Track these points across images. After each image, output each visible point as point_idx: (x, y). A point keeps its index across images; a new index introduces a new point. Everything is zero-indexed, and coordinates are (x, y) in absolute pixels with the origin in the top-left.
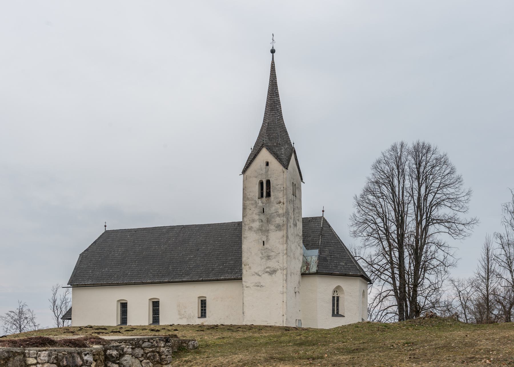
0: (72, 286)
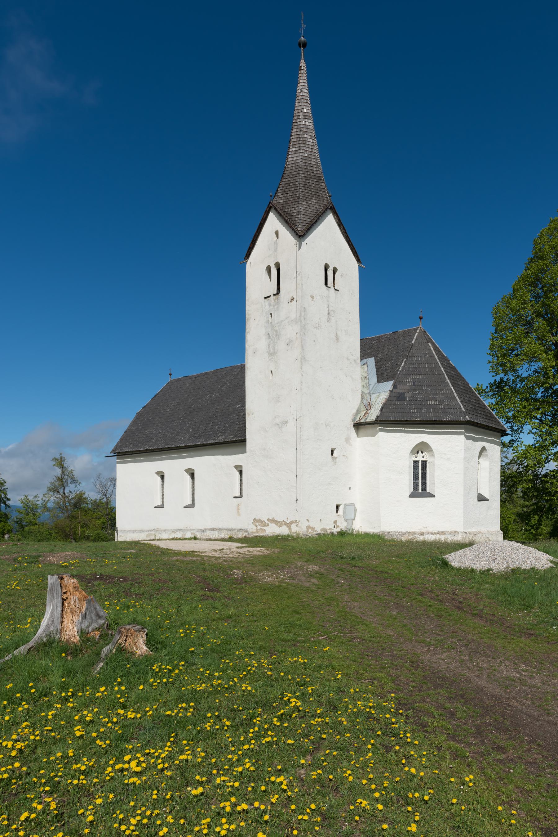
0: (116, 454)
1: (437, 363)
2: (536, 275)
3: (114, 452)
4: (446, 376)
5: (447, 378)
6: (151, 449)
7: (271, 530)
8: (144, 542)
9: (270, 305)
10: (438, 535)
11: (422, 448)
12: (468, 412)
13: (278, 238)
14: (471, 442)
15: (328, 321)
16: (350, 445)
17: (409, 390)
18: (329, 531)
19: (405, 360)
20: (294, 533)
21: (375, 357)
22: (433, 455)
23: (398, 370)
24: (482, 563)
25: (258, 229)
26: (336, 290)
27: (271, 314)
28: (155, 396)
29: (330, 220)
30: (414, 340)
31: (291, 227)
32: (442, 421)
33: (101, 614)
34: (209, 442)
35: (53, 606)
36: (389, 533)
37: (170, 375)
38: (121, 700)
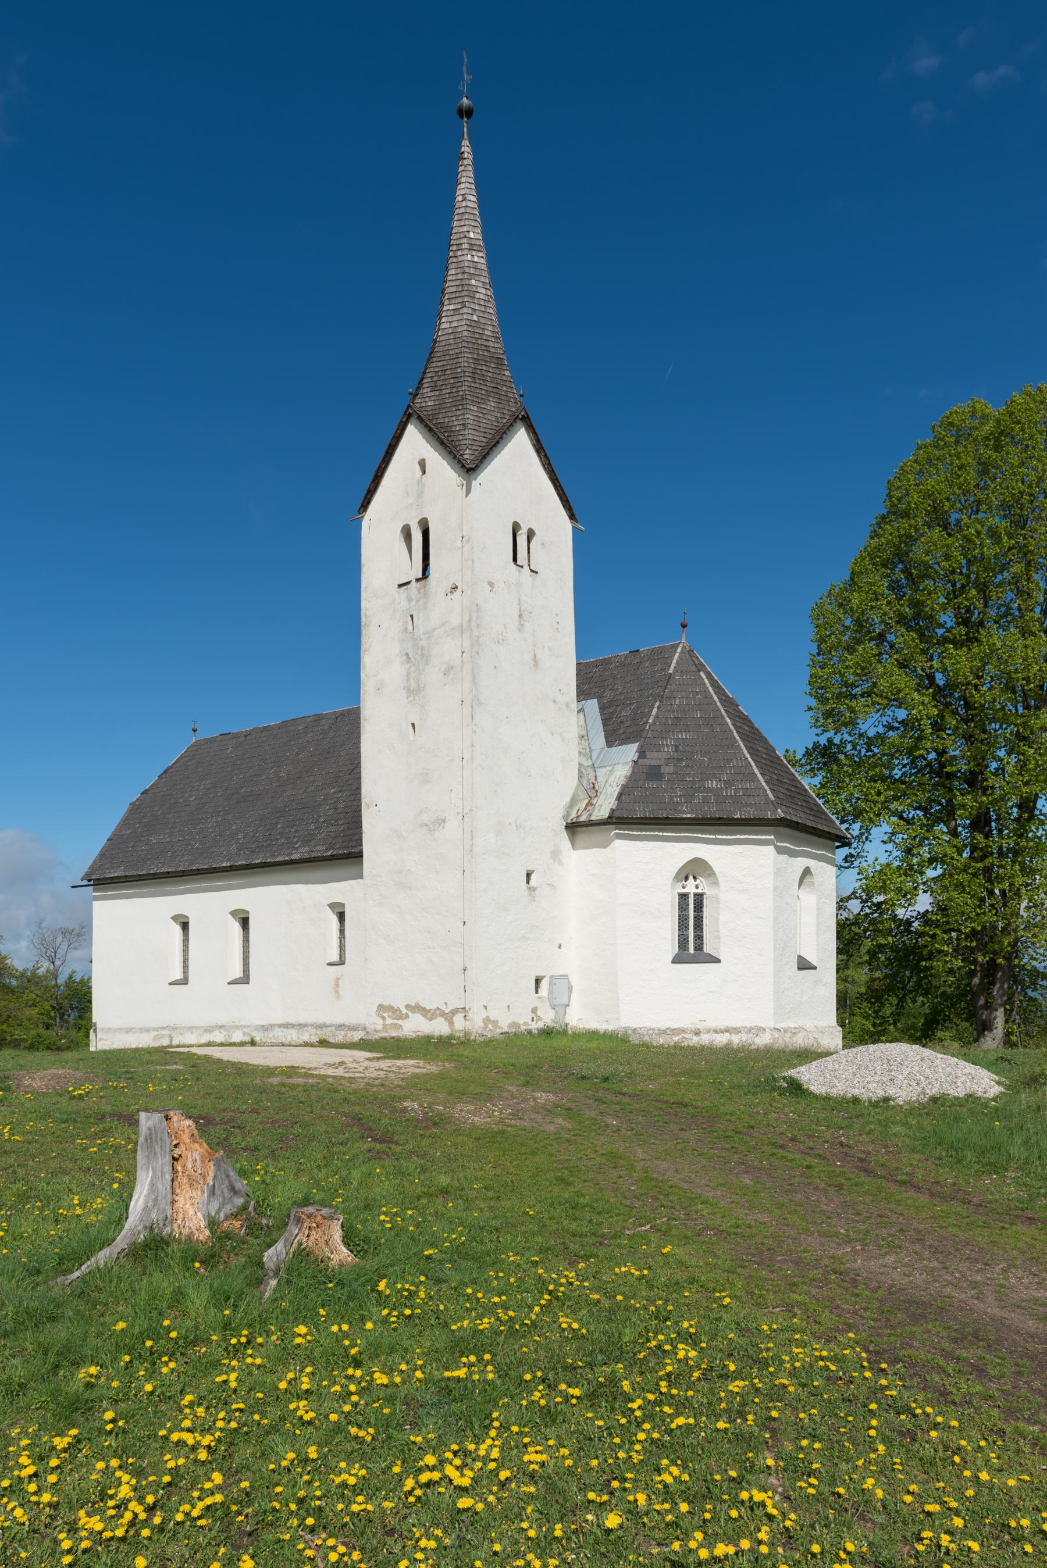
1: (719, 710)
2: (895, 545)
3: (87, 877)
4: (736, 735)
5: (738, 738)
6: (163, 873)
7: (414, 1026)
8: (178, 1050)
9: (409, 599)
10: (727, 1035)
11: (695, 869)
12: (779, 802)
13: (424, 472)
14: (784, 857)
15: (519, 630)
16: (561, 864)
17: (668, 761)
18: (523, 1028)
19: (658, 704)
20: (460, 1031)
21: (599, 698)
22: (716, 884)
23: (646, 723)
24: (870, 1086)
25: (385, 456)
26: (532, 571)
27: (412, 616)
28: (166, 772)
29: (521, 439)
30: (672, 667)
31: (451, 453)
32: (733, 819)
33: (238, 1185)
34: (280, 859)
35: (154, 1171)
36: (635, 1030)
37: (195, 730)
38: (353, 1351)
